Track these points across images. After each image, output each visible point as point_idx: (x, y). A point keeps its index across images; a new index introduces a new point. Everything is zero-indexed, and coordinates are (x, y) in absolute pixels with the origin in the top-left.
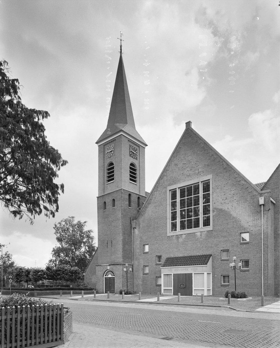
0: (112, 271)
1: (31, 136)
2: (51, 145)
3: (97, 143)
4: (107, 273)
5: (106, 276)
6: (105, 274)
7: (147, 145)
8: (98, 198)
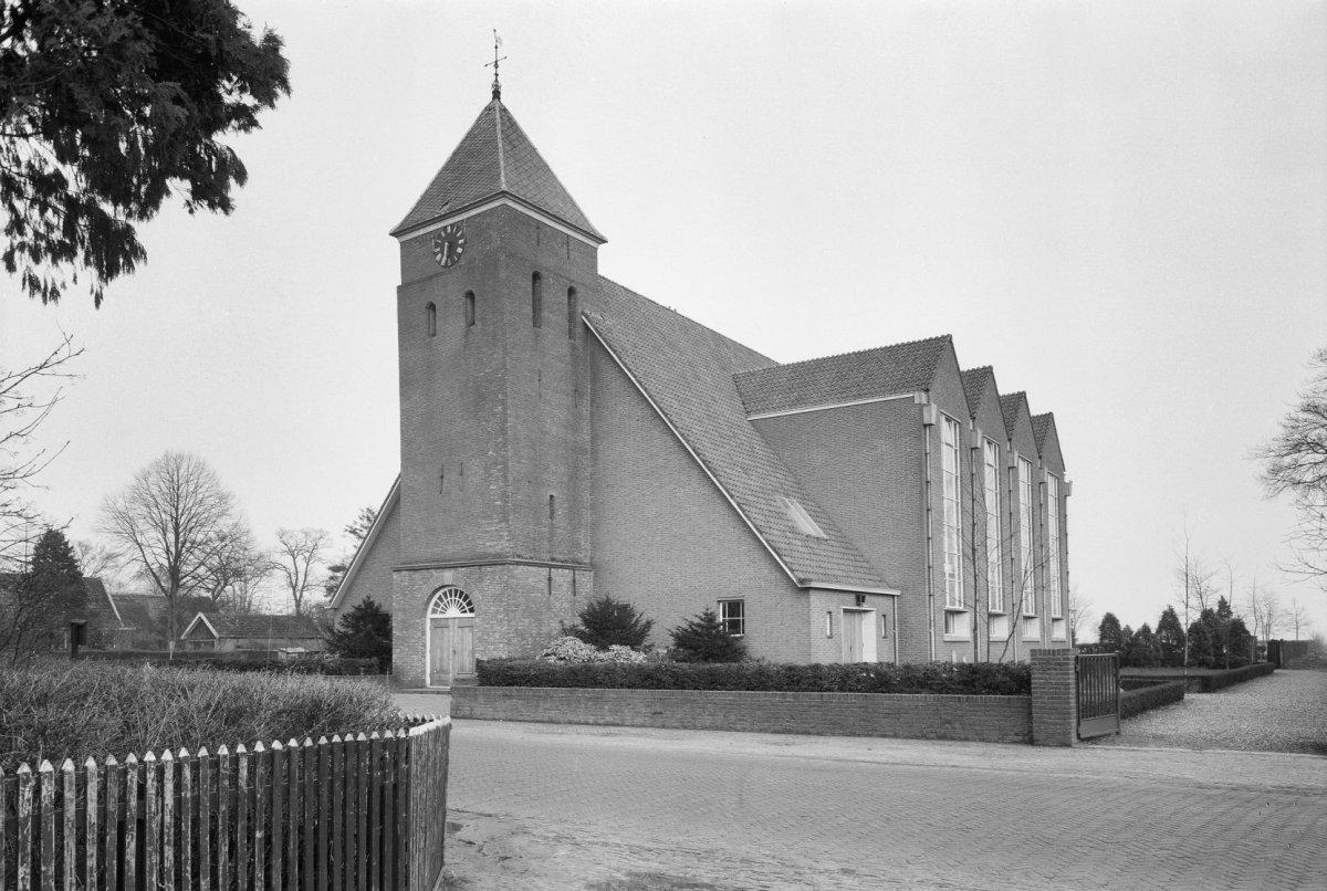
0: (462, 593)
1: (719, 625)
2: (611, 265)
3: (395, 234)
4: (440, 598)
5: (434, 611)
6: (431, 605)
7: (602, 241)
8: (399, 287)
